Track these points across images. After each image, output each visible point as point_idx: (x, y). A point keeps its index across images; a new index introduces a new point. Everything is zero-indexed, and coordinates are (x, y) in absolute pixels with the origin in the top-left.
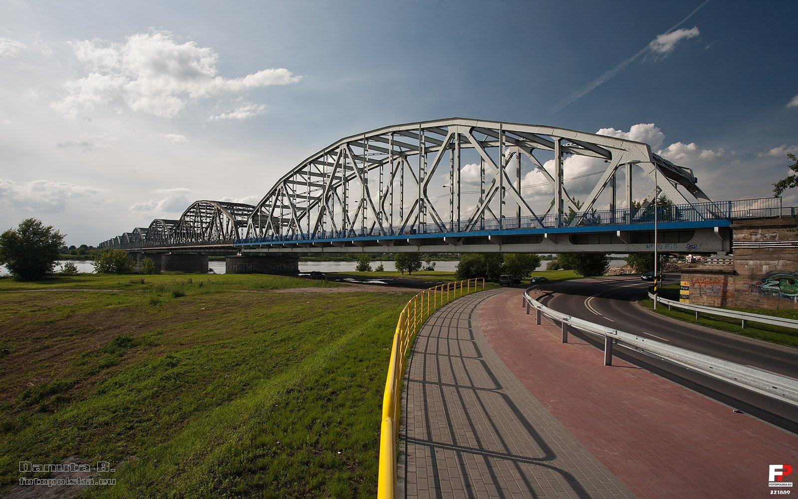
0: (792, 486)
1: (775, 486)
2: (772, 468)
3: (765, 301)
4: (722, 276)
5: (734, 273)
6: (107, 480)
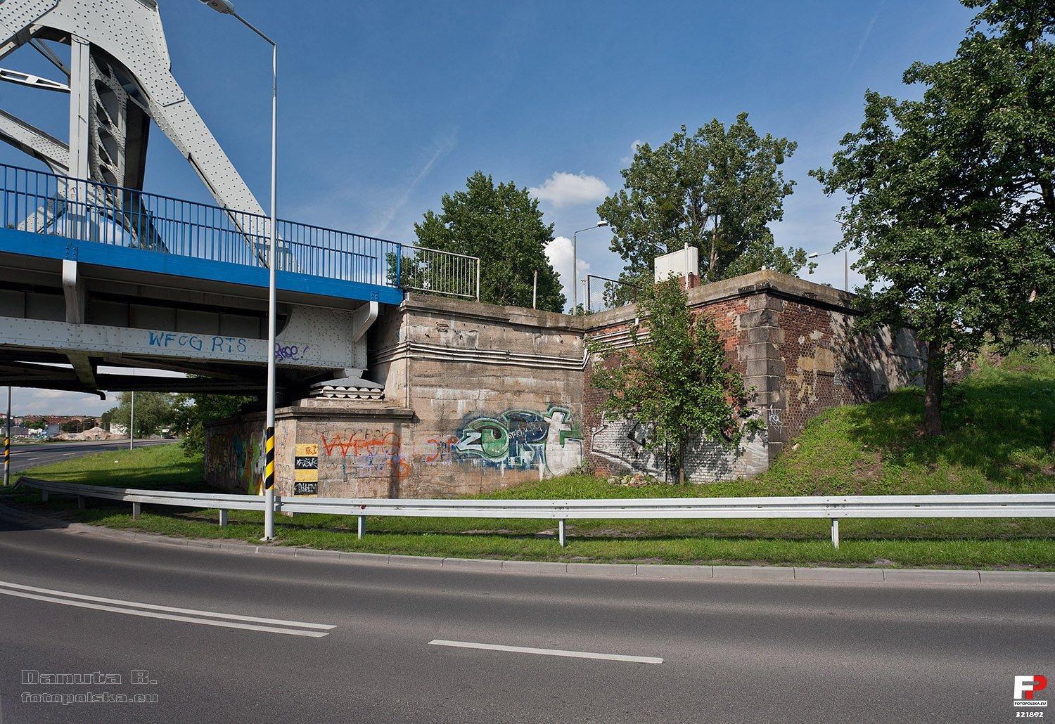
0: (1046, 705)
1: (1022, 706)
2: (1019, 680)
3: (463, 476)
4: (390, 426)
5: (412, 418)
6: (145, 696)
